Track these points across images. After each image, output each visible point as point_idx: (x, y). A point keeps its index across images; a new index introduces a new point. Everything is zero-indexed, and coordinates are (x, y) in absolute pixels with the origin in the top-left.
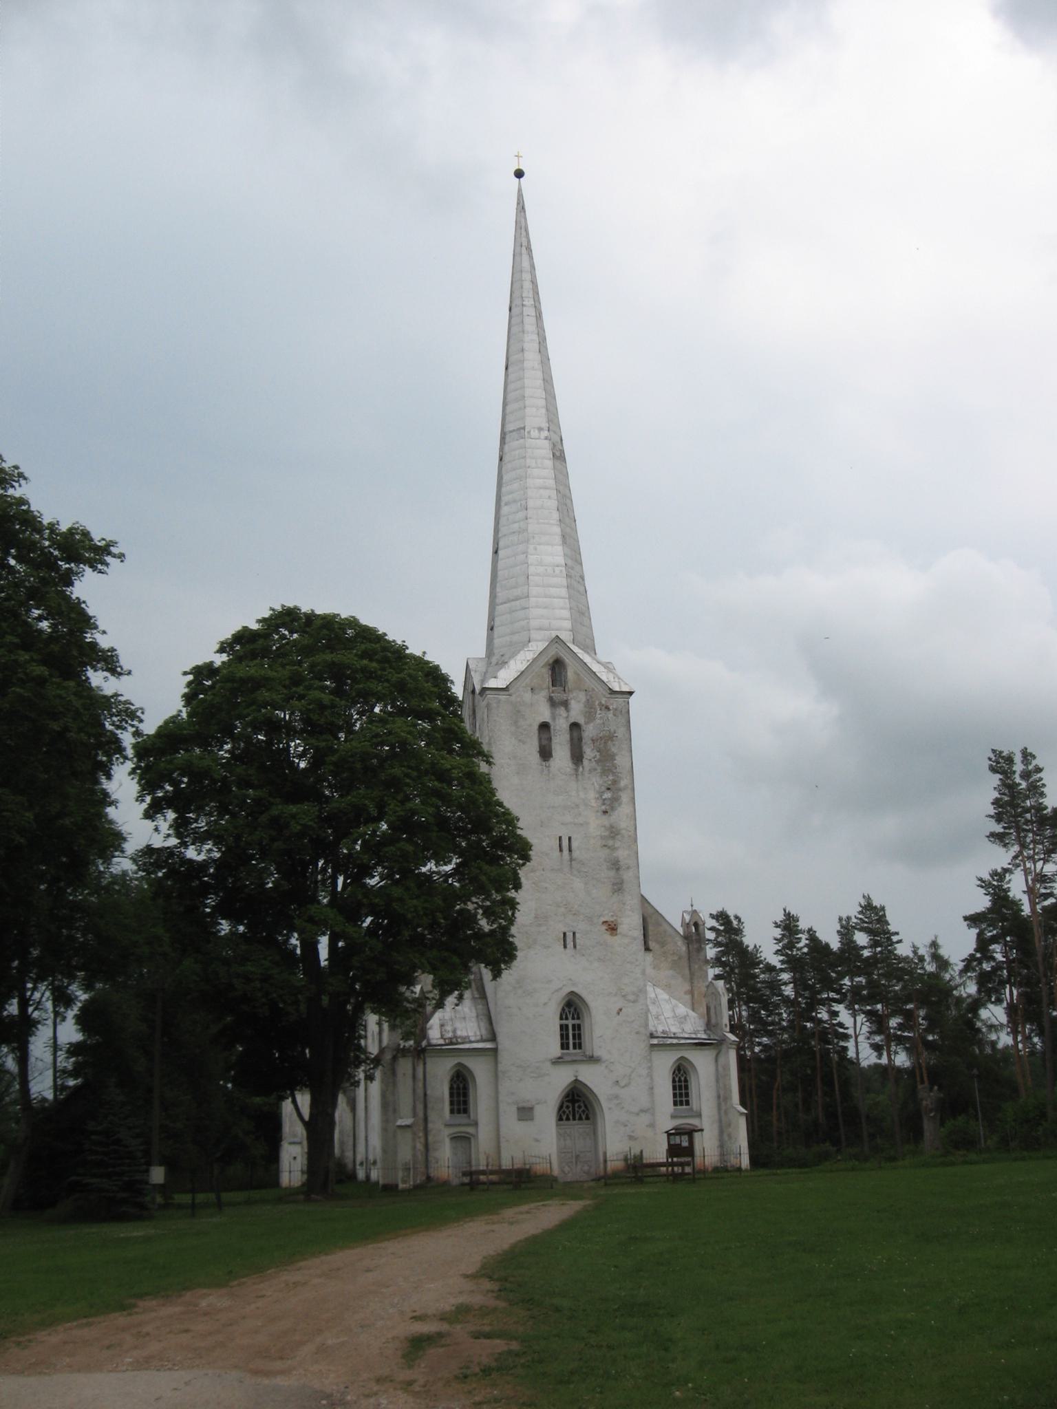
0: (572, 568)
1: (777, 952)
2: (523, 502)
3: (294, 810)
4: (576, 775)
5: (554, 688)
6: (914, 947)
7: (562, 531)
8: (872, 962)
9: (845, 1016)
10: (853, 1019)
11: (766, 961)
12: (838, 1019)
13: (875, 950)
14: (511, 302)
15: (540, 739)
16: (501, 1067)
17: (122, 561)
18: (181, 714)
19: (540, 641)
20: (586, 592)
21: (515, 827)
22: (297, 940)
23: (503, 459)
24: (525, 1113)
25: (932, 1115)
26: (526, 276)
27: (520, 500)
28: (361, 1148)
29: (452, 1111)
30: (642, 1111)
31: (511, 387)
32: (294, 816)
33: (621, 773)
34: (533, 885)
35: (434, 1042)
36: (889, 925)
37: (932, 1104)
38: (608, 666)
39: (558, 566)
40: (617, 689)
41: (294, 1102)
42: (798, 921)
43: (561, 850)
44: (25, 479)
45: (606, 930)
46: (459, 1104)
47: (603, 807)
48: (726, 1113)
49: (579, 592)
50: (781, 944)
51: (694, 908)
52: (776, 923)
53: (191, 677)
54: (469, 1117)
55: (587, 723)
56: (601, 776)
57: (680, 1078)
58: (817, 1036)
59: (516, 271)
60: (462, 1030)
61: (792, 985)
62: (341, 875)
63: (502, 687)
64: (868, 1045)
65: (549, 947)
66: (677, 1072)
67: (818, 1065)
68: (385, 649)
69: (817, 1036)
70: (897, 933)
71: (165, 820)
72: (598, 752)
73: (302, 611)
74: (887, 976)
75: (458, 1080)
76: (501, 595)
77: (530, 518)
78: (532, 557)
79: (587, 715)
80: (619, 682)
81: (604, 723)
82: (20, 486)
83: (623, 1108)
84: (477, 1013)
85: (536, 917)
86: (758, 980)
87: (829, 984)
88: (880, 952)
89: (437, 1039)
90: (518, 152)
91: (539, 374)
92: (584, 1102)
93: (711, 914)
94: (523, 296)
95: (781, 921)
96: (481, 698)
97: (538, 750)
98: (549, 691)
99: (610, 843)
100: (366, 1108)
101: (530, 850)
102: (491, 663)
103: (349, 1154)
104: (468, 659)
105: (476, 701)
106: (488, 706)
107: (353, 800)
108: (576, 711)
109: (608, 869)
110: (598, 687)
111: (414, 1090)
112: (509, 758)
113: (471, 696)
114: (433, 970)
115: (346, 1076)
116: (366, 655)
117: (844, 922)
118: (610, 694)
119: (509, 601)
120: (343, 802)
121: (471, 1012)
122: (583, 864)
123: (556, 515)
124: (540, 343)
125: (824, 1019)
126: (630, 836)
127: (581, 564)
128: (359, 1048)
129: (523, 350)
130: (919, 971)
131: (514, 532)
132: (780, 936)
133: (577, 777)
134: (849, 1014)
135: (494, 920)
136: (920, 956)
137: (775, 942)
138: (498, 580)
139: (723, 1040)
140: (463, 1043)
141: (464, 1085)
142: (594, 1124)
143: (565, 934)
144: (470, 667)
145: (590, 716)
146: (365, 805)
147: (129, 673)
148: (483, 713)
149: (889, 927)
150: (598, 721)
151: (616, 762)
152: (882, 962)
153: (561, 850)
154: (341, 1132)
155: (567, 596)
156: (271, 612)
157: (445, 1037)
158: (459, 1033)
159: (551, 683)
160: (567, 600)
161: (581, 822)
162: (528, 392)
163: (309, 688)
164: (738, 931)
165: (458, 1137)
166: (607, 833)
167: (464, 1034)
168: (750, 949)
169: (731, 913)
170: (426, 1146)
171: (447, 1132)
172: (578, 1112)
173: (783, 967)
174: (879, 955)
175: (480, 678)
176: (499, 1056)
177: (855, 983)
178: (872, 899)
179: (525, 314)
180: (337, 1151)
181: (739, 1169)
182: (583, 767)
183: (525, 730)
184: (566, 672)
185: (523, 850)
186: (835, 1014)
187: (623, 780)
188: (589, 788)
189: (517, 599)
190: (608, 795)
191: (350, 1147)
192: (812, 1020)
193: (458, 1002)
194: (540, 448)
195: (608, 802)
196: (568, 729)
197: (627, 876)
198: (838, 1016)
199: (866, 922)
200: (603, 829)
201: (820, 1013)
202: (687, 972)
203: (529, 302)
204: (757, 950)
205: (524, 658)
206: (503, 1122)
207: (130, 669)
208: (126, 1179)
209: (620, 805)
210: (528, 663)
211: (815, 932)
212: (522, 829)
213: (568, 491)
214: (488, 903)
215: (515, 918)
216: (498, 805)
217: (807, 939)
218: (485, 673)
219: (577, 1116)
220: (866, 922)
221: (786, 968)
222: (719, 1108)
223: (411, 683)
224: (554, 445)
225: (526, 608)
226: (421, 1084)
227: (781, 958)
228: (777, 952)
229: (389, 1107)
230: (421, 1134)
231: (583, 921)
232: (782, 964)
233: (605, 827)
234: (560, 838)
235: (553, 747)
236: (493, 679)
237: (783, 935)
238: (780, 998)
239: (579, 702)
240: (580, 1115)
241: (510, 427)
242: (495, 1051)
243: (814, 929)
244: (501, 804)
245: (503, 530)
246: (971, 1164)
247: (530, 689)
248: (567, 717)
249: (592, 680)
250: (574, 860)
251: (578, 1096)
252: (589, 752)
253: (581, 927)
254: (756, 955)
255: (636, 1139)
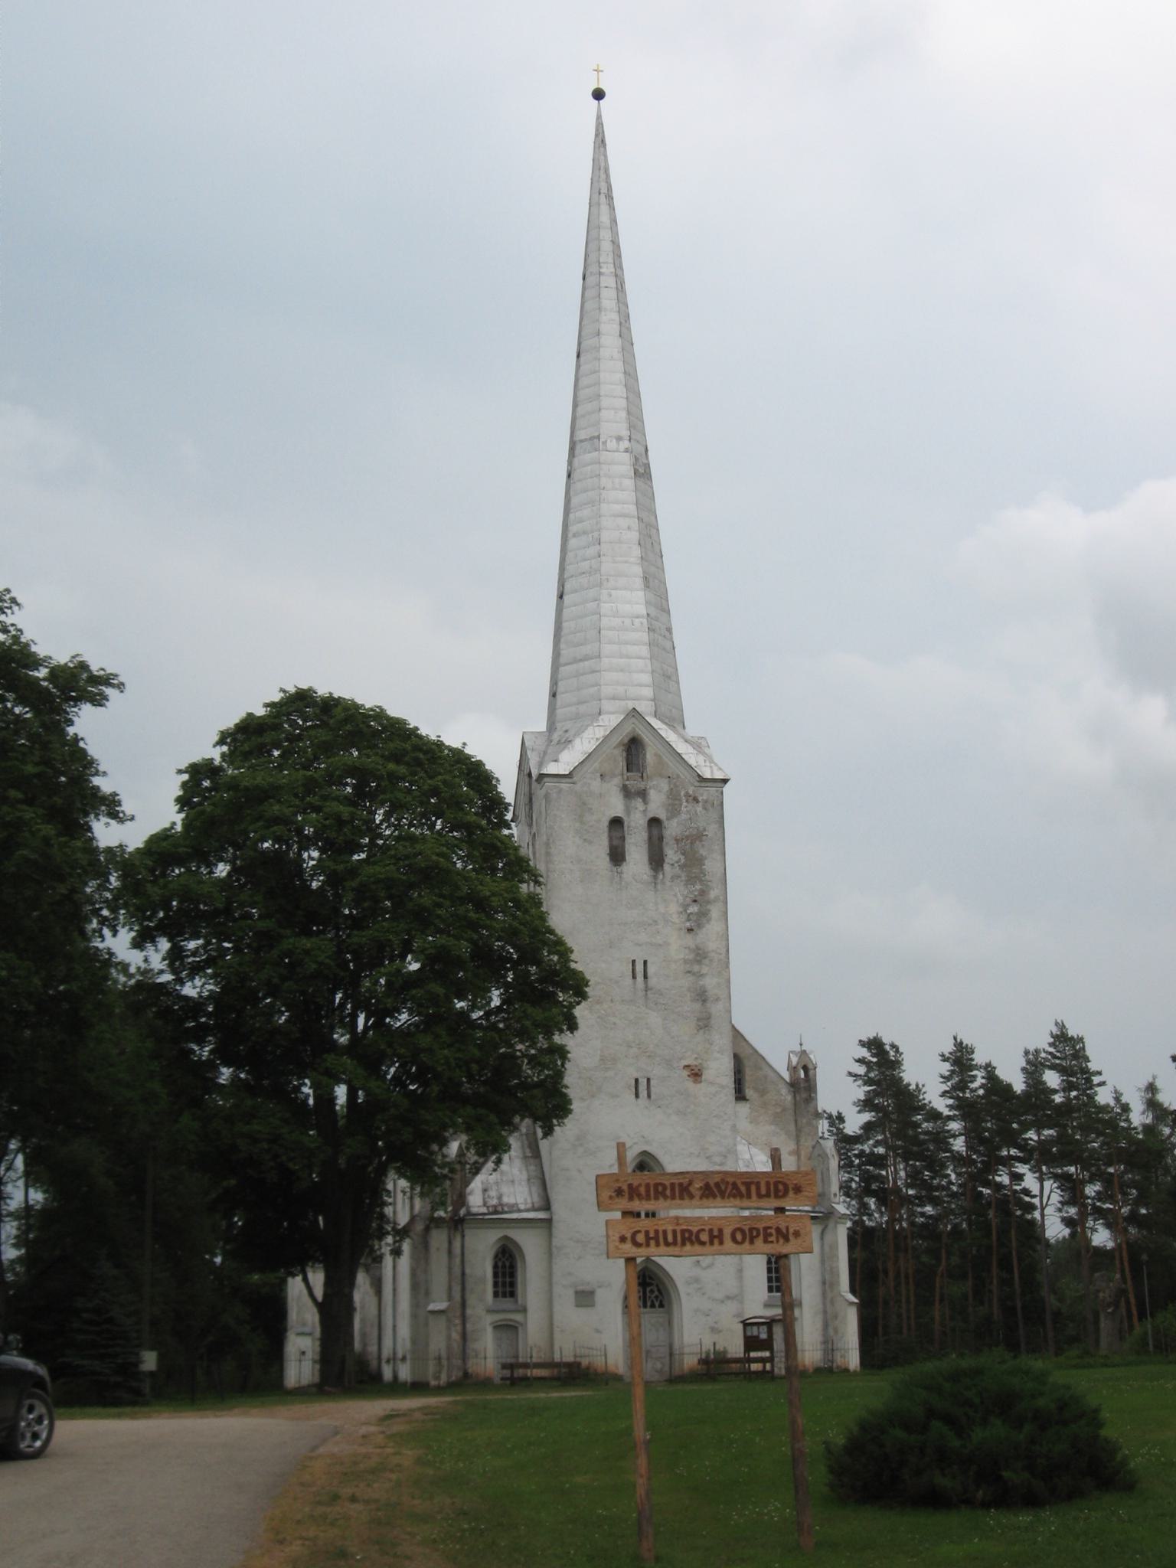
0: (657, 619)
1: (944, 1094)
2: (596, 534)
3: (309, 945)
4: (655, 884)
5: (629, 774)
6: (1116, 1092)
7: (644, 572)
8: (1066, 1109)
9: (1030, 1182)
10: (1038, 1185)
11: (931, 1105)
12: (1023, 1184)
13: (1069, 1095)
14: (585, 268)
15: (611, 838)
16: (555, 1242)
17: (122, 692)
18: (175, 827)
19: (613, 713)
20: (674, 648)
21: (568, 960)
22: (310, 1088)
23: (572, 476)
24: (585, 1297)
25: (1110, 1310)
26: (606, 235)
27: (592, 532)
28: (387, 1343)
29: (496, 1294)
30: (728, 1298)
31: (584, 382)
32: (307, 952)
33: (710, 881)
34: (598, 1020)
35: (474, 1210)
36: (1089, 1061)
37: (1110, 1296)
38: (698, 745)
39: (637, 617)
40: (708, 775)
41: (305, 1280)
42: (973, 1052)
43: (634, 977)
44: (18, 604)
45: (689, 1076)
46: (504, 1284)
47: (688, 924)
48: (832, 1302)
49: (664, 649)
50: (949, 1084)
51: (804, 1048)
52: (943, 1055)
53: (186, 777)
54: (516, 1301)
55: (668, 819)
56: (686, 885)
57: (504, 1262)
58: (993, 1205)
59: (592, 226)
60: (508, 1196)
61: (963, 1138)
62: (362, 1013)
63: (563, 773)
64: (1060, 1220)
65: (617, 1096)
66: (500, 1255)
67: (995, 1244)
68: (416, 748)
69: (993, 1205)
70: (1099, 1073)
71: (157, 950)
72: (683, 854)
73: (319, 694)
74: (1085, 1129)
75: (504, 1256)
76: (566, 653)
77: (604, 555)
78: (605, 604)
79: (670, 808)
80: (711, 767)
81: (690, 819)
82: (13, 613)
83: (704, 1294)
84: (529, 1176)
85: (601, 1060)
86: (920, 1130)
87: (1013, 1139)
88: (1075, 1097)
89: (479, 1206)
90: (598, 65)
91: (620, 365)
92: (657, 1286)
93: (860, 1041)
94: (601, 261)
95: (950, 1053)
96: (539, 786)
97: (608, 852)
98: (623, 778)
99: (696, 968)
100: (395, 1290)
101: (587, 985)
102: (551, 741)
103: (373, 1349)
104: (524, 733)
105: (533, 787)
106: (547, 796)
107: (376, 934)
108: (657, 804)
109: (692, 1001)
110: (686, 773)
111: (450, 1269)
112: (572, 862)
113: (527, 780)
114: (468, 1129)
115: (367, 1250)
116: (397, 757)
117: (1031, 1057)
118: (698, 781)
119: (576, 661)
120: (364, 936)
121: (521, 1173)
122: (662, 994)
123: (637, 552)
124: (621, 324)
125: (1004, 1183)
126: (720, 960)
127: (668, 612)
128: (382, 1216)
129: (598, 334)
130: (1122, 1124)
131: (584, 573)
132: (948, 1073)
133: (655, 887)
134: (1035, 1177)
135: (541, 1071)
136: (1123, 1104)
137: (942, 1080)
138: (563, 634)
139: (830, 1213)
140: (506, 1213)
141: (511, 1263)
142: (670, 1313)
143: (637, 1081)
144: (526, 744)
145: (674, 811)
146: (390, 940)
147: (132, 818)
148: (541, 804)
149: (1088, 1064)
150: (684, 816)
151: (704, 867)
152: (1079, 1110)
153: (634, 977)
154: (363, 1320)
155: (649, 656)
156: (282, 695)
157: (488, 1205)
158: (505, 1200)
159: (625, 768)
160: (648, 662)
161: (661, 942)
162: (604, 389)
163: (325, 798)
164: (896, 1064)
165: (504, 1325)
166: (691, 956)
167: (512, 1201)
168: (913, 1087)
169: (886, 1040)
170: (464, 1336)
171: (489, 1319)
172: (650, 1297)
173: (951, 1113)
174: (1074, 1102)
175: (537, 759)
176: (554, 1230)
177: (1043, 1138)
178: (1067, 1027)
179: (602, 285)
180: (357, 1345)
181: (847, 1370)
182: (663, 874)
183: (591, 826)
184: (645, 754)
185: (578, 987)
186: (1017, 1177)
187: (714, 890)
188: (671, 899)
189: (586, 658)
190: (694, 909)
191: (375, 1341)
192: (987, 1184)
193: (496, 1167)
194: (620, 464)
195: (694, 918)
196: (646, 825)
197: (716, 1009)
198: (1023, 1180)
199: (1058, 1058)
200: (687, 951)
201: (1000, 1175)
202: (792, 1127)
203: (608, 269)
204: (920, 1091)
205: (591, 736)
206: (557, 1308)
207: (133, 813)
208: (120, 1361)
209: (709, 921)
210: (598, 743)
211: (995, 1068)
212: (576, 962)
213: (653, 518)
214: (533, 1052)
215: (565, 1069)
216: (549, 933)
217: (983, 1078)
218: (545, 753)
219: (649, 1304)
220: (1058, 1058)
221: (955, 1115)
222: (824, 1294)
223: (446, 792)
224: (636, 459)
225: (597, 671)
226: (458, 1261)
227: (951, 1102)
228: (944, 1094)
229: (420, 1288)
230: (457, 1321)
231: (659, 1064)
232: (950, 1111)
233: (689, 948)
234: (634, 962)
235: (626, 850)
236: (554, 763)
237: (953, 1072)
238: (947, 1154)
239: (660, 791)
240: (652, 1301)
241: (581, 435)
242: (548, 1222)
243: (994, 1064)
244: (552, 932)
245: (570, 569)
246: (1114, 1366)
247: (599, 775)
248: (645, 811)
249: (678, 764)
250: (651, 989)
251: (651, 1278)
252: (671, 854)
253: (657, 1071)
254: (917, 1097)
255: (720, 1331)
